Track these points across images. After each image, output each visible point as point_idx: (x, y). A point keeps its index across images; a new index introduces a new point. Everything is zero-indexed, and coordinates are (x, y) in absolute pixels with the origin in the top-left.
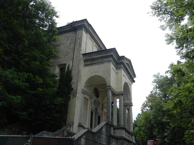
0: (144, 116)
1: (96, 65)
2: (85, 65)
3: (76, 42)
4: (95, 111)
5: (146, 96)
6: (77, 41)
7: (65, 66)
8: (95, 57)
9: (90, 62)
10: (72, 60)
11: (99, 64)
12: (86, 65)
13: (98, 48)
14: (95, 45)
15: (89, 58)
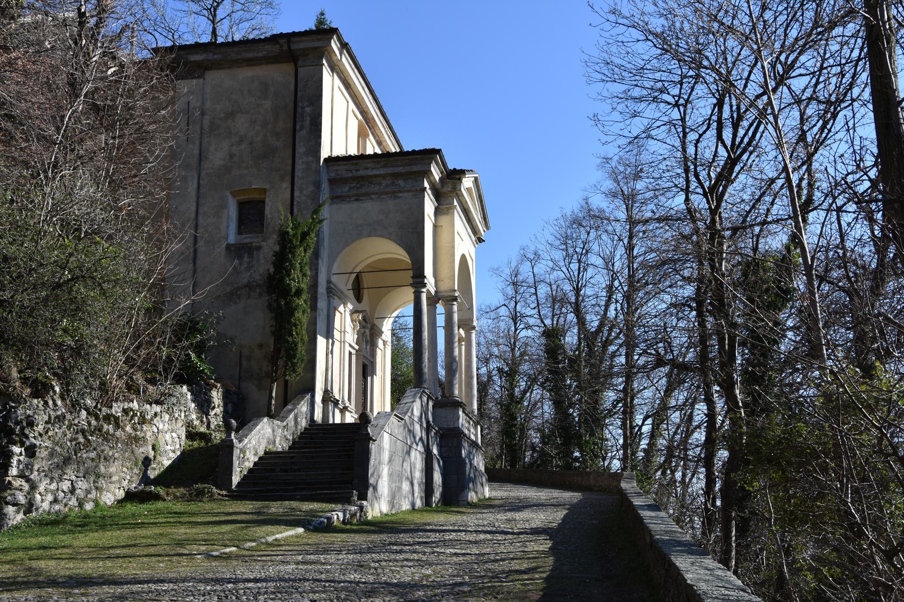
0: (639, 514)
1: (372, 199)
2: (336, 199)
3: (299, 109)
4: (357, 347)
5: (333, 21)
6: (303, 108)
7: (262, 196)
8: (370, 173)
9: (350, 188)
10: (289, 178)
11: (382, 196)
12: (337, 197)
13: (360, 117)
14: (353, 111)
15: (350, 175)
